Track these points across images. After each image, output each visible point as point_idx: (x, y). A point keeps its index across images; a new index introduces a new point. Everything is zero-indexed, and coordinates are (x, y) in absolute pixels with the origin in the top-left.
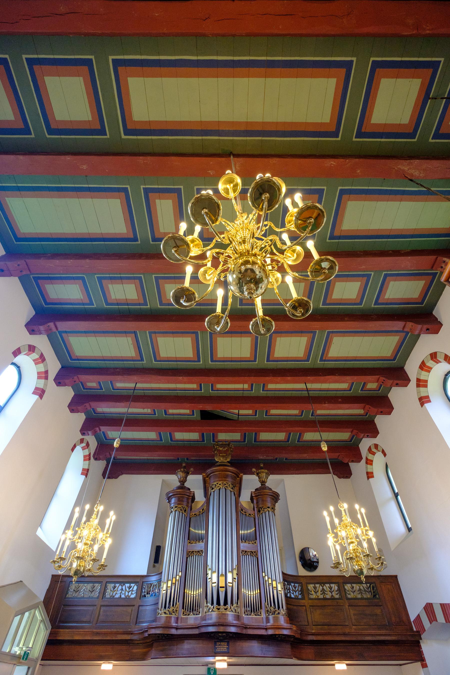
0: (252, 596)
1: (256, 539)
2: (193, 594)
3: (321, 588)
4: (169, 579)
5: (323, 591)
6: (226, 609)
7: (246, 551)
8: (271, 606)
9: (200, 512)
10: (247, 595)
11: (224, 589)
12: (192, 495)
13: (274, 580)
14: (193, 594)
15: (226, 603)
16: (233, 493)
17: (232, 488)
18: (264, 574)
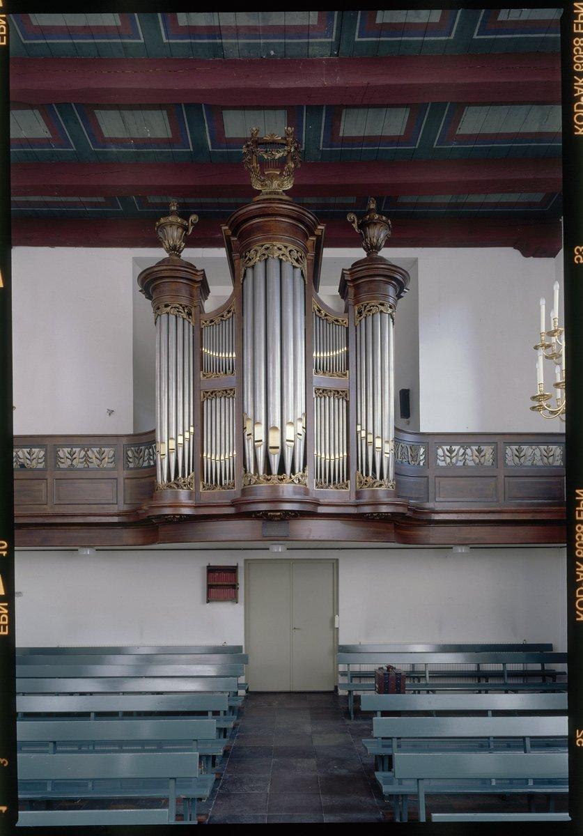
0: (332, 461)
1: (348, 369)
2: (330, 459)
3: (83, 453)
4: (179, 433)
5: (87, 459)
6: (281, 480)
7: (324, 390)
8: (367, 475)
9: (223, 316)
10: (323, 460)
11: (279, 450)
12: (200, 279)
13: (378, 437)
14: (330, 459)
15: (282, 469)
16: (298, 272)
17: (297, 260)
18: (359, 427)
